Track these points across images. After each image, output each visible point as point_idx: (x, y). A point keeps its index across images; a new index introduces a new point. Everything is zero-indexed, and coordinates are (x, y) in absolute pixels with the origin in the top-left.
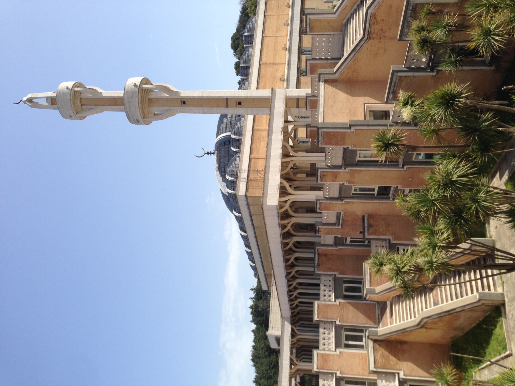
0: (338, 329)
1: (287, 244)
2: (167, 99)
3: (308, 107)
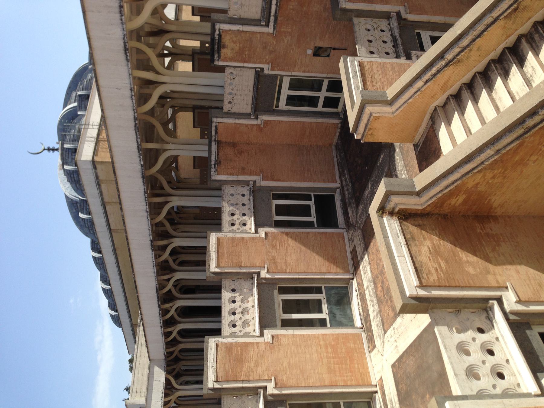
0: (265, 287)
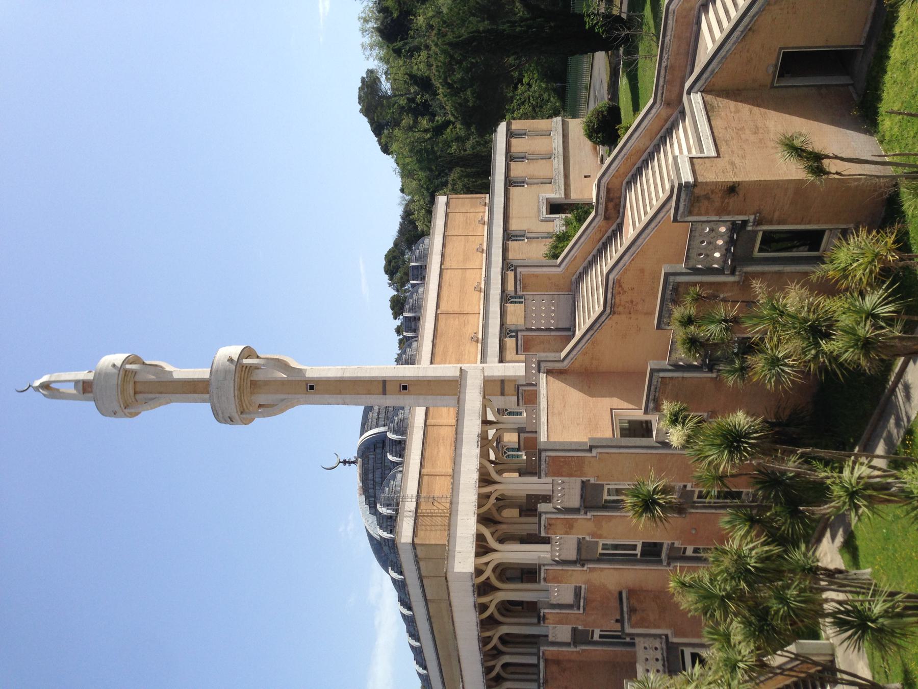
1: (490, 638)
2: (283, 382)
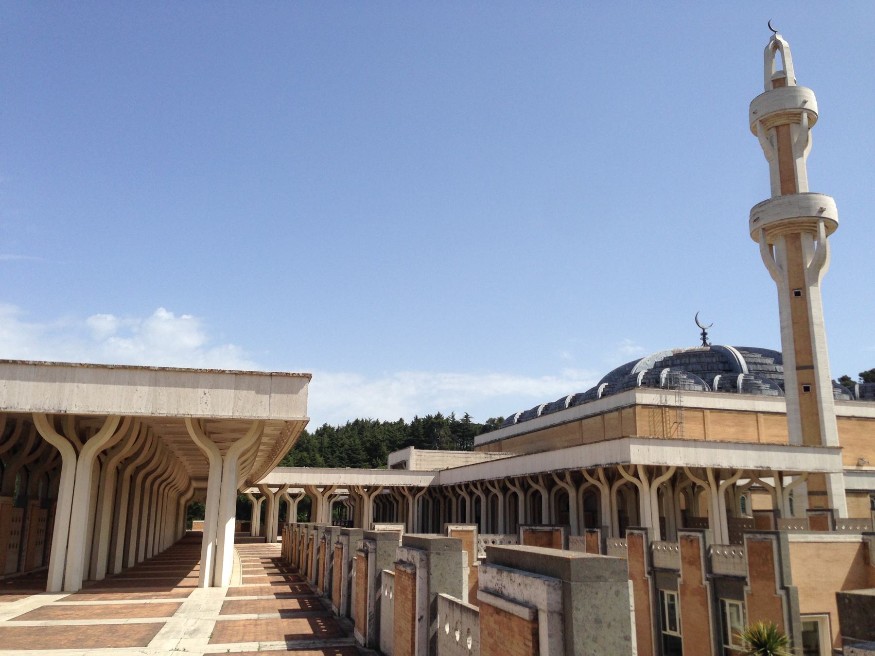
1: (537, 482)
2: (801, 265)
3: (813, 513)
